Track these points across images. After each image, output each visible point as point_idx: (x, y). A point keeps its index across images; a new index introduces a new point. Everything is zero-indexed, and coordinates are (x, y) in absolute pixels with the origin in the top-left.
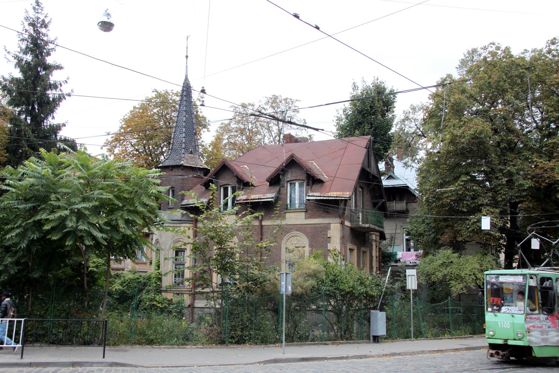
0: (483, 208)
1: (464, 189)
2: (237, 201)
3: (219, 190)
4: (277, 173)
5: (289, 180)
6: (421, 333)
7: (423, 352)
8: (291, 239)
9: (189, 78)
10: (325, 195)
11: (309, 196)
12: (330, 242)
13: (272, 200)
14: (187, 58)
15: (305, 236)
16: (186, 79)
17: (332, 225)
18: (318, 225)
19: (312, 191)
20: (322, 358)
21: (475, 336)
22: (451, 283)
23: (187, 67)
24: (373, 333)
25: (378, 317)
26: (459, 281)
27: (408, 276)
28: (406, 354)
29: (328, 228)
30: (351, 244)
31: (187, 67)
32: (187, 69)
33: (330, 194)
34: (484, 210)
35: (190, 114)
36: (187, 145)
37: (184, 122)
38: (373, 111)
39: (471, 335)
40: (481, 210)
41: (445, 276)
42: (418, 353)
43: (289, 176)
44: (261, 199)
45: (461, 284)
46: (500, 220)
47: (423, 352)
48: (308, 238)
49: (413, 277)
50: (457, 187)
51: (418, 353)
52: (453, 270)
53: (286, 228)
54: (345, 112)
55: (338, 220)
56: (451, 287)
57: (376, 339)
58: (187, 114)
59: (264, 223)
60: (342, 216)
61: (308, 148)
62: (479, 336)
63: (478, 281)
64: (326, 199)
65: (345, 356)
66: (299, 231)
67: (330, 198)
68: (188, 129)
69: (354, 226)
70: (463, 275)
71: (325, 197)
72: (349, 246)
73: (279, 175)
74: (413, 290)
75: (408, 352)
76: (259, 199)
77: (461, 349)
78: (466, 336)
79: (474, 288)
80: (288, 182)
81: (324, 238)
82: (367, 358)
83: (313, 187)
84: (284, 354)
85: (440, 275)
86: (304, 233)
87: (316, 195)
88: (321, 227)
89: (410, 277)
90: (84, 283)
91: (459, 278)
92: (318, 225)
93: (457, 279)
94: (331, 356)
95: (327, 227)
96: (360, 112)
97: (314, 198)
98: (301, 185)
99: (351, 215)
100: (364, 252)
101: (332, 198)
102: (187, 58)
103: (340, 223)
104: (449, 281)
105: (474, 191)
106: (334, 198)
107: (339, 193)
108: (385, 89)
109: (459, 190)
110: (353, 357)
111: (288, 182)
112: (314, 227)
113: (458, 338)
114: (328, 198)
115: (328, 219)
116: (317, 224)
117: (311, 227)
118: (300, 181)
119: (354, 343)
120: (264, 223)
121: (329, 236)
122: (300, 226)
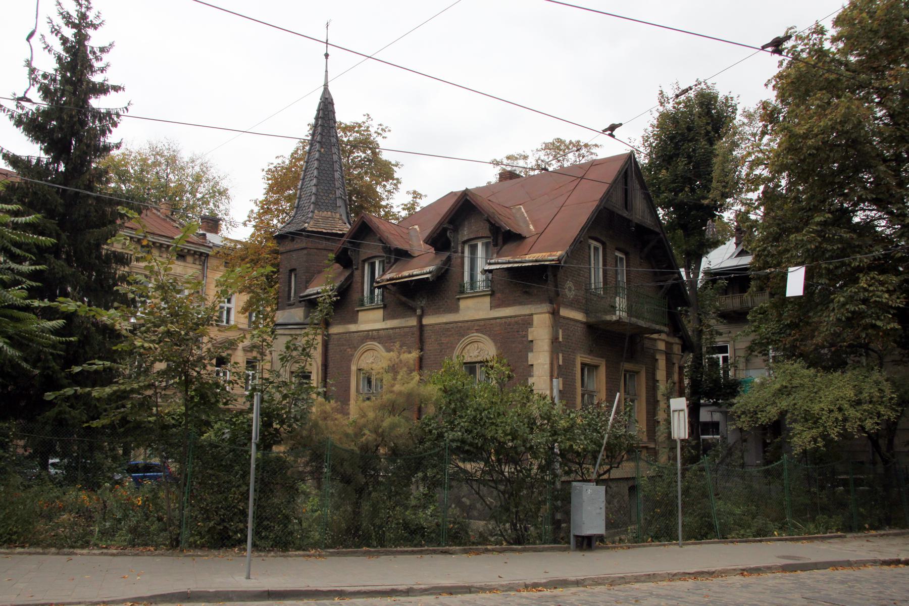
0: (861, 275)
1: (819, 239)
2: (378, 282)
4: (441, 228)
5: (465, 238)
6: (711, 527)
8: (468, 347)
9: (330, 89)
10: (517, 260)
12: (532, 351)
17: (535, 317)
18: (513, 320)
19: (499, 254)
21: (849, 535)
24: (574, 532)
25: (585, 498)
26: (810, 423)
27: (674, 411)
28: (597, 582)
29: (529, 324)
30: (589, 354)
33: (528, 258)
36: (320, 197)
37: (317, 159)
38: (691, 135)
39: (839, 533)
40: (858, 278)
41: (783, 414)
43: (465, 233)
46: (898, 298)
47: (651, 577)
48: (496, 345)
49: (682, 414)
50: (805, 235)
52: (798, 400)
53: (461, 327)
54: (647, 141)
55: (546, 307)
56: (794, 435)
57: (587, 543)
59: (426, 321)
60: (555, 300)
64: (518, 267)
65: (400, 588)
66: (482, 333)
67: (524, 265)
68: (324, 172)
69: (592, 320)
72: (580, 359)
73: (445, 230)
74: (682, 440)
77: (769, 569)
78: (828, 535)
80: (464, 243)
82: (470, 592)
83: (505, 247)
84: (248, 578)
86: (489, 336)
87: (506, 260)
88: (516, 323)
89: (676, 414)
91: (812, 419)
93: (807, 420)
95: (527, 322)
96: (672, 138)
97: (498, 266)
100: (634, 374)
101: (527, 264)
103: (549, 312)
104: (790, 423)
105: (841, 240)
106: (530, 264)
107: (544, 254)
108: (715, 98)
109: (810, 242)
111: (464, 243)
114: (520, 265)
116: (511, 317)
118: (485, 240)
119: (524, 550)
120: (426, 321)
121: (530, 338)
122: (482, 323)
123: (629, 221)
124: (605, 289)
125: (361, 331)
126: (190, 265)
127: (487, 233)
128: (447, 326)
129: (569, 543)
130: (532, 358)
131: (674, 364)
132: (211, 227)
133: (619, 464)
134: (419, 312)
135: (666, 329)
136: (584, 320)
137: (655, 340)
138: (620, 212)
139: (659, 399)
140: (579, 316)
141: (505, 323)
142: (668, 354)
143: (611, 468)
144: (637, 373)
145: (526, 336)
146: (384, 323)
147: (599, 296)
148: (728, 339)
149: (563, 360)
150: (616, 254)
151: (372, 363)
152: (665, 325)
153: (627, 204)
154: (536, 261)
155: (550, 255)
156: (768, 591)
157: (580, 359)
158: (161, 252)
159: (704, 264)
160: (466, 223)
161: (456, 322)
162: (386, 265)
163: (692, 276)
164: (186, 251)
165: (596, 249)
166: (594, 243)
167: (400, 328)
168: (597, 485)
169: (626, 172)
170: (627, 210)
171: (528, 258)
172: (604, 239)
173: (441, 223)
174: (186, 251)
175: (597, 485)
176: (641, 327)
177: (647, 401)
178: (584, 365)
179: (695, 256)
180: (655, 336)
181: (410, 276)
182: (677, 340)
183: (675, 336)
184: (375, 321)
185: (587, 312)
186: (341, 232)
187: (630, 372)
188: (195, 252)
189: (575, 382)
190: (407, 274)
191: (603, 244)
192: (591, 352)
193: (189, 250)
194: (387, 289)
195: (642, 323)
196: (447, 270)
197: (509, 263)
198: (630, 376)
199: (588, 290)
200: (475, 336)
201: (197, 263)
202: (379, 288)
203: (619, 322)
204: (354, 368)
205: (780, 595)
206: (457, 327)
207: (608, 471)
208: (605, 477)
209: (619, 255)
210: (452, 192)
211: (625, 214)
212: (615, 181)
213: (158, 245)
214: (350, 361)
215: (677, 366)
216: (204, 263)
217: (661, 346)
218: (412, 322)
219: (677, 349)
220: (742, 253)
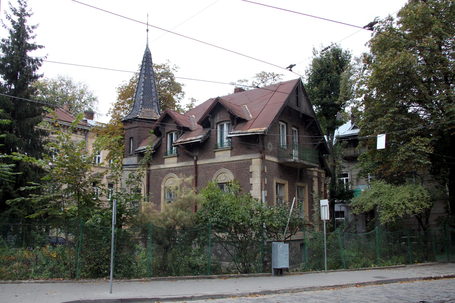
0: (412, 138)
2: (174, 144)
3: (165, 137)
5: (218, 121)
7: (312, 289)
8: (220, 176)
9: (150, 47)
10: (243, 132)
11: (230, 134)
12: (252, 177)
14: (147, 32)
15: (231, 172)
16: (147, 48)
17: (253, 160)
20: (152, 299)
21: (408, 266)
22: (381, 213)
23: (147, 38)
24: (274, 266)
25: (279, 250)
30: (280, 178)
31: (147, 38)
32: (147, 41)
33: (249, 131)
34: (414, 139)
35: (149, 76)
36: (145, 101)
37: (143, 82)
39: (403, 265)
40: (411, 139)
41: (375, 206)
42: (305, 290)
44: (192, 140)
45: (391, 214)
46: (430, 149)
47: (312, 289)
49: (326, 207)
51: (305, 290)
52: (383, 200)
53: (216, 166)
55: (258, 155)
57: (280, 272)
58: (146, 76)
59: (198, 163)
60: (263, 152)
61: (246, 95)
62: (413, 265)
63: (407, 211)
64: (244, 135)
65: (188, 296)
66: (227, 168)
67: (247, 134)
69: (281, 161)
70: (392, 204)
73: (208, 117)
74: (326, 220)
75: (290, 290)
77: (369, 283)
78: (398, 266)
80: (217, 124)
81: (247, 173)
82: (223, 298)
83: (238, 126)
84: (111, 293)
85: (370, 205)
86: (230, 170)
87: (239, 132)
88: (244, 163)
89: (323, 207)
91: (389, 208)
92: (242, 162)
93: (387, 209)
94: (166, 297)
95: (249, 163)
97: (234, 135)
98: (228, 125)
99: (279, 152)
101: (249, 134)
102: (147, 32)
103: (260, 158)
107: (257, 129)
110: (200, 297)
111: (217, 124)
113: (386, 268)
115: (250, 155)
116: (241, 160)
118: (228, 122)
119: (249, 276)
120: (198, 163)
121: (251, 171)
122: (227, 163)
124: (287, 146)
125: (166, 168)
126: (79, 136)
128: (209, 165)
130: (252, 181)
131: (322, 183)
133: (295, 232)
134: (195, 158)
135: (318, 166)
136: (277, 161)
137: (312, 171)
138: (294, 108)
140: (275, 160)
141: (238, 163)
142: (319, 178)
143: (291, 235)
144: (304, 187)
145: (249, 170)
146: (177, 164)
148: (348, 170)
150: (293, 129)
153: (298, 104)
154: (253, 132)
155: (260, 130)
156: (369, 294)
158: (64, 129)
159: (336, 133)
161: (213, 163)
163: (330, 139)
164: (77, 129)
165: (283, 126)
166: (281, 123)
167: (185, 166)
168: (284, 243)
169: (297, 88)
171: (249, 131)
172: (286, 121)
173: (205, 114)
174: (77, 129)
175: (284, 243)
178: (277, 184)
179: (331, 130)
180: (312, 169)
181: (190, 140)
182: (323, 171)
183: (322, 169)
184: (173, 163)
185: (278, 158)
186: (155, 119)
190: (189, 140)
191: (286, 123)
192: (281, 177)
193: (78, 128)
195: (305, 163)
197: (240, 133)
198: (300, 189)
199: (279, 147)
200: (223, 170)
201: (83, 134)
202: (175, 146)
204: (163, 187)
205: (375, 296)
206: (214, 166)
207: (290, 236)
208: (289, 239)
211: (297, 109)
214: (161, 183)
215: (323, 184)
216: (86, 135)
217: (315, 174)
218: (192, 163)
219: (323, 175)
220: (354, 128)
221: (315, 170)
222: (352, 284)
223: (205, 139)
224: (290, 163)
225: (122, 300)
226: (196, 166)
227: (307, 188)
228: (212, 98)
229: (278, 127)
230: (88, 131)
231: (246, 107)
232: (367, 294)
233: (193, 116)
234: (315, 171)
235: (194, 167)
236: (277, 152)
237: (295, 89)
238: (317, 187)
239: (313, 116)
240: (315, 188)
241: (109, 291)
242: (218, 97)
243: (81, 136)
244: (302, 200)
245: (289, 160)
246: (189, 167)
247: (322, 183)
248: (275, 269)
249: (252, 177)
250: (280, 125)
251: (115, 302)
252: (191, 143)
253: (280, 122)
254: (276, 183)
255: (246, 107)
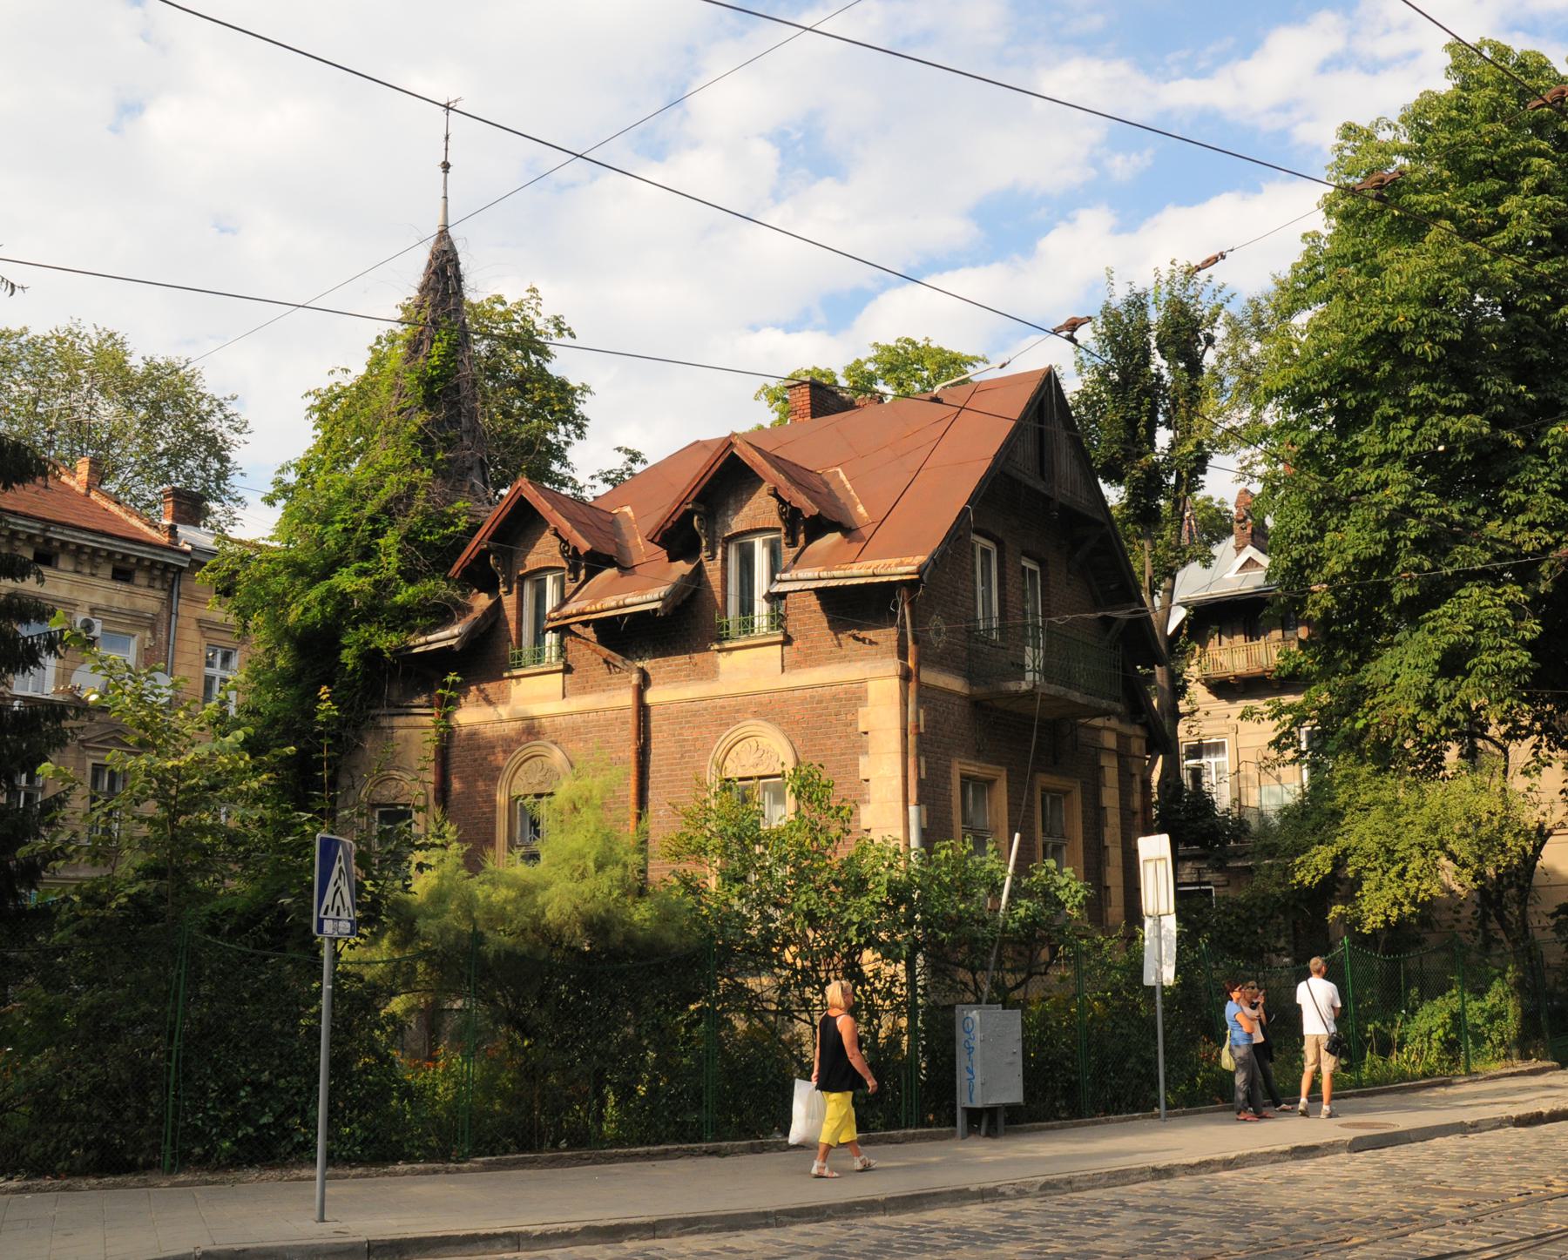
13: (658, 605)
16: (444, 234)
17: (871, 685)
24: (963, 1101)
29: (860, 698)
30: (976, 758)
31: (446, 197)
32: (446, 206)
67: (849, 582)
69: (980, 691)
71: (834, 578)
73: (688, 515)
76: (618, 607)
79: (388, 655)
88: (835, 698)
90: (331, 1077)
95: (855, 697)
100: (1056, 798)
106: (862, 581)
112: (812, 697)
114: (841, 583)
115: (860, 664)
117: (804, 700)
121: (862, 728)
123: (1048, 499)
124: (1002, 629)
126: (142, 591)
127: (774, 520)
128: (694, 706)
129: (954, 1124)
130: (865, 766)
131: (1134, 775)
132: (186, 513)
135: (1120, 708)
136: (966, 691)
137: (1098, 729)
138: (1031, 483)
139: (1107, 843)
140: (955, 684)
142: (1123, 755)
143: (1030, 975)
144: (1067, 793)
145: (852, 724)
147: (993, 645)
148: (1225, 730)
149: (927, 769)
150: (1024, 563)
151: (540, 783)
152: (1117, 700)
155: (901, 564)
156: (1336, 1186)
157: (959, 767)
158: (78, 562)
160: (731, 501)
161: (712, 698)
162: (568, 584)
164: (133, 560)
165: (986, 553)
166: (981, 542)
168: (1004, 1008)
169: (1042, 403)
170: (1044, 479)
171: (856, 569)
172: (999, 534)
174: (133, 560)
175: (1004, 1008)
176: (1076, 704)
177: (1085, 848)
178: (966, 779)
180: (1098, 722)
182: (1138, 730)
183: (1133, 722)
185: (970, 676)
187: (1054, 791)
188: (153, 563)
189: (951, 813)
190: (613, 604)
191: (999, 543)
192: (979, 754)
193: (140, 560)
194: (572, 633)
195: (1077, 696)
196: (695, 593)
198: (1053, 799)
199: (971, 632)
200: (751, 725)
201: (158, 584)
202: (554, 630)
203: (1031, 694)
204: (501, 799)
205: (1359, 1190)
209: (1028, 564)
210: (698, 442)
211: (1040, 487)
212: (1025, 415)
213: (72, 547)
214: (494, 780)
215: (1138, 778)
216: (172, 587)
217: (1110, 741)
219: (1137, 746)
221: (1108, 724)
222: (1268, 1153)
223: (679, 603)
224: (1018, 696)
225: (373, 1248)
226: (643, 711)
227: (1077, 797)
228: (702, 438)
229: (969, 556)
230: (181, 569)
231: (842, 476)
232: (1327, 1185)
233: (627, 509)
234: (1108, 729)
235: (631, 715)
236: (964, 654)
237: (1034, 408)
238: (1117, 792)
239: (1100, 517)
240: (1110, 797)
241: (316, 1215)
242: (733, 435)
243: (152, 592)
244: (1060, 841)
245: (1012, 686)
246: (613, 715)
247: (1134, 775)
248: (964, 1109)
249: (867, 753)
250: (973, 550)
251: (325, 1256)
252: (622, 616)
253: (975, 538)
254: (962, 776)
255: (842, 476)
